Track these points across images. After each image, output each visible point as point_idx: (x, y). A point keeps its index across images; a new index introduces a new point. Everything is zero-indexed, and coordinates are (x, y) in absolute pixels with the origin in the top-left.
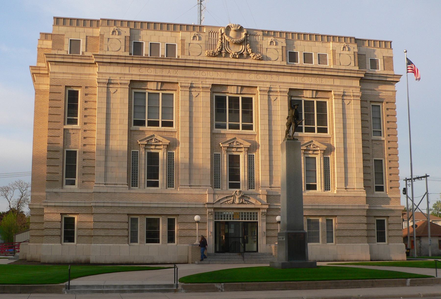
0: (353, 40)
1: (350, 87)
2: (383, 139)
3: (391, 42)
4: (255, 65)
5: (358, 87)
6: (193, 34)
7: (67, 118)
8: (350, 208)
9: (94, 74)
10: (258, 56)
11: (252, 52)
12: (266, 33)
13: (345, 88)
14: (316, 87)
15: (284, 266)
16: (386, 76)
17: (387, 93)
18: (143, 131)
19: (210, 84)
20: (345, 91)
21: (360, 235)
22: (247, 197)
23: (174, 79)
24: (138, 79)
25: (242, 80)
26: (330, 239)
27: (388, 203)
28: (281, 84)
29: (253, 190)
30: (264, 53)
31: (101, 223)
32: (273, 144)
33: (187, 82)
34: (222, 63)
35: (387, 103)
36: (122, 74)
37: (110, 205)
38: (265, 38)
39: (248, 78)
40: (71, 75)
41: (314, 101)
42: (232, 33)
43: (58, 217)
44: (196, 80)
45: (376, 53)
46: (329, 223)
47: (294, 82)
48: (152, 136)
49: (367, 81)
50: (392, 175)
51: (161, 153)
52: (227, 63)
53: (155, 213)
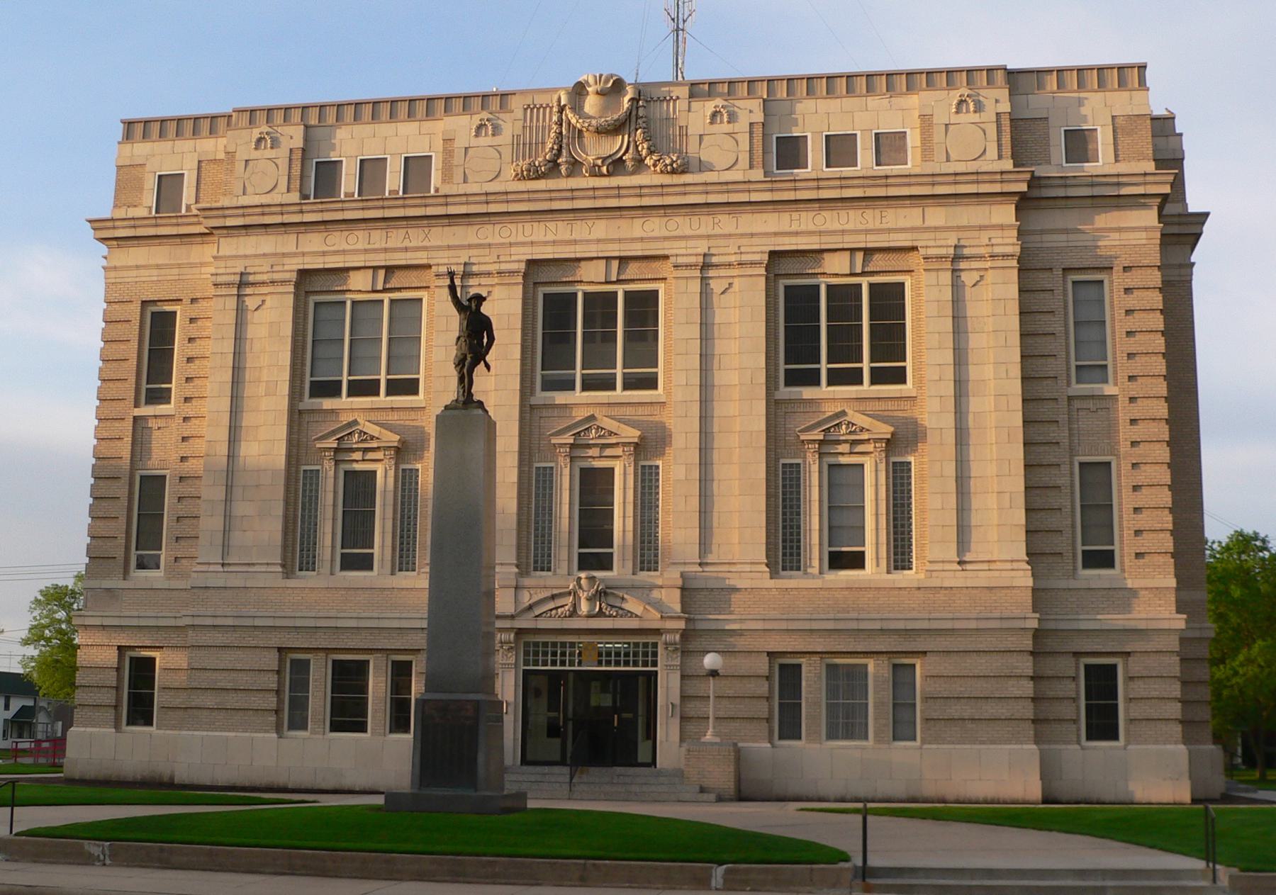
0: (1000, 76)
1: (981, 228)
2: (1109, 389)
3: (1142, 67)
4: (653, 190)
5: (1010, 226)
6: (955, 96)
7: (144, 386)
8: (973, 625)
9: (209, 262)
10: (668, 162)
11: (651, 152)
12: (698, 90)
13: (961, 235)
14: (862, 238)
15: (394, 800)
16: (1115, 180)
17: (1125, 235)
18: (333, 411)
19: (519, 261)
20: (962, 243)
21: (1008, 715)
22: (617, 596)
23: (419, 254)
24: (321, 266)
25: (620, 240)
26: (902, 728)
27: (1126, 607)
28: (745, 241)
29: (906, 572)
30: (692, 148)
31: (208, 674)
32: (716, 429)
33: (694, 251)
34: (553, 195)
35: (1126, 269)
36: (275, 255)
37: (230, 622)
38: (695, 105)
39: (638, 233)
40: (155, 272)
41: (860, 285)
42: (591, 104)
43: (111, 657)
44: (481, 252)
45: (1084, 111)
46: (901, 674)
47: (787, 229)
48: (837, 415)
49: (1051, 203)
50: (1145, 514)
51: (380, 469)
52: (569, 194)
53: (351, 645)
